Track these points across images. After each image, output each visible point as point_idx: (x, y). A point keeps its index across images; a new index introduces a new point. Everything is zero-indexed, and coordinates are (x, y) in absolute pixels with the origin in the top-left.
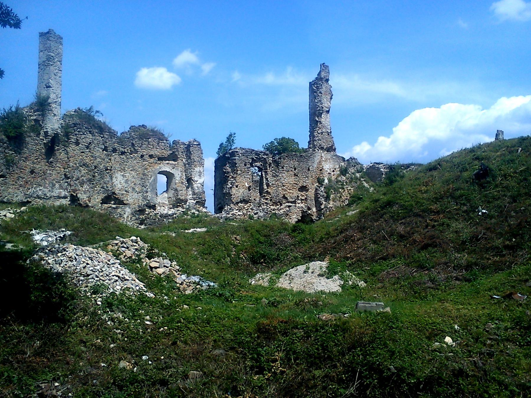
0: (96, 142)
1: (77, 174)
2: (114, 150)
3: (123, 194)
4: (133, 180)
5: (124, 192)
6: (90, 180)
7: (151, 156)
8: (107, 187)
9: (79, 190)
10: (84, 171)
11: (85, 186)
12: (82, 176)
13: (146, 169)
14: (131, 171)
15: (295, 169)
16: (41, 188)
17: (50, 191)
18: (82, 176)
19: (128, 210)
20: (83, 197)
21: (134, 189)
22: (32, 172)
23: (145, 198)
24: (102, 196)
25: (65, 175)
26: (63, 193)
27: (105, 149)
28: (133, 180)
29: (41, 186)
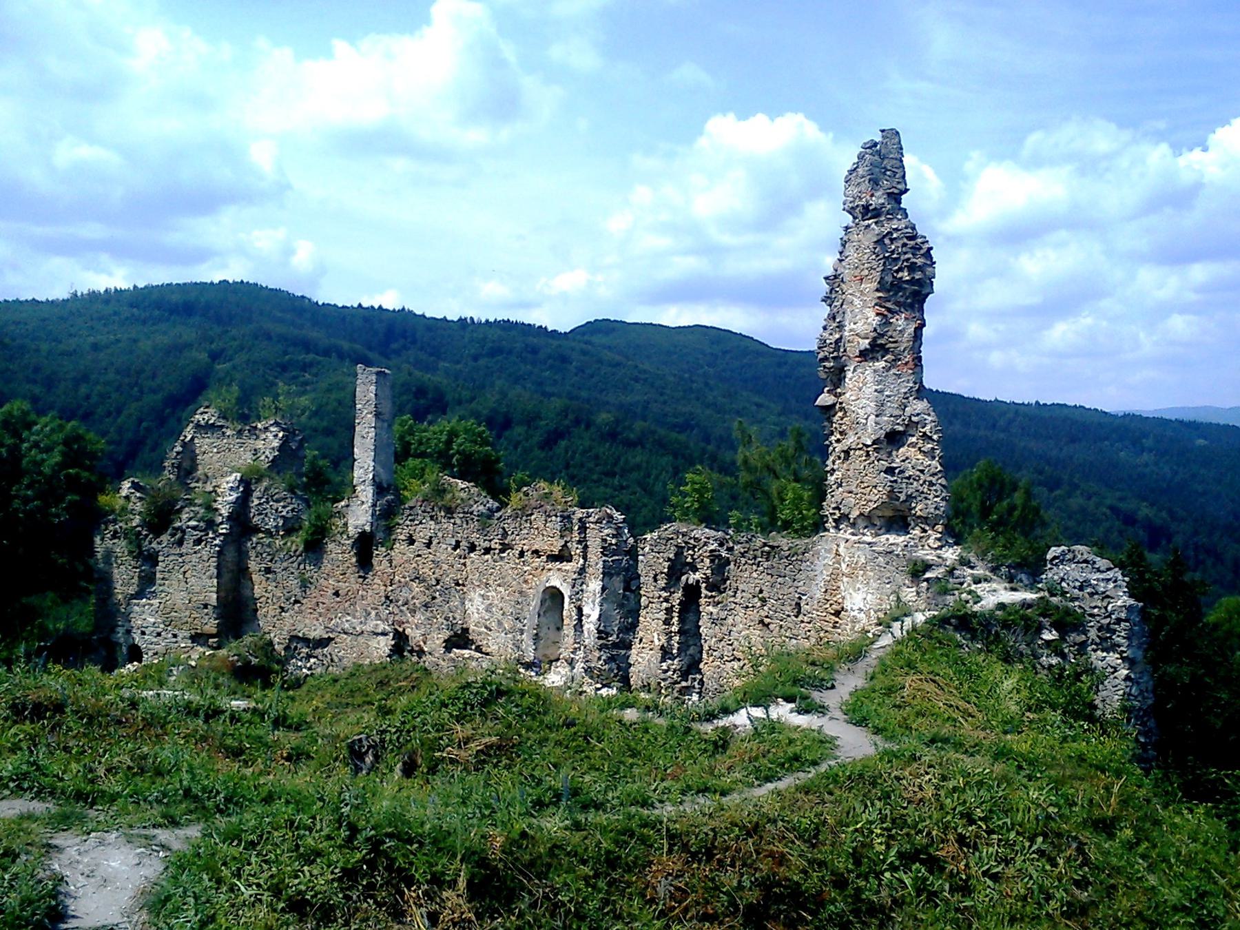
0: (440, 534)
1: (405, 594)
2: (472, 548)
3: (480, 634)
5: (483, 629)
6: (426, 606)
7: (536, 553)
11: (418, 615)
13: (526, 582)
15: (764, 601)
20: (415, 635)
21: (500, 623)
22: (337, 594)
24: (446, 634)
25: (387, 597)
26: (382, 626)
27: (457, 546)
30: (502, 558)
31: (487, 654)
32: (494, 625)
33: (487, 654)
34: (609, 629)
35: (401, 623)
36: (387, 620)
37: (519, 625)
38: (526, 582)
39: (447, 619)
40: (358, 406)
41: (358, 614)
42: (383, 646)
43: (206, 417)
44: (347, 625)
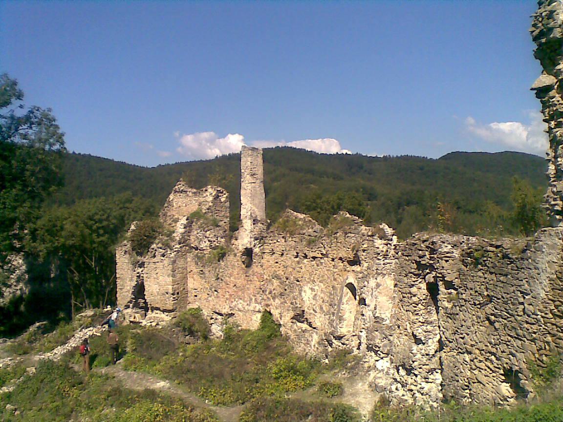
2: (306, 257)
4: (322, 295)
5: (312, 311)
6: (281, 295)
7: (341, 259)
8: (296, 303)
9: (271, 304)
10: (276, 282)
12: (274, 289)
13: (335, 279)
14: (320, 282)
16: (241, 301)
17: (248, 305)
18: (274, 289)
19: (315, 338)
21: (321, 308)
23: (331, 323)
24: (291, 314)
28: (322, 295)
29: (241, 299)
30: (321, 263)
31: (314, 328)
32: (318, 310)
33: (314, 328)
34: (383, 316)
35: (268, 305)
36: (261, 303)
37: (332, 310)
38: (335, 279)
39: (292, 303)
40: (243, 171)
41: (246, 299)
42: (254, 322)
43: (179, 186)
44: (240, 306)
